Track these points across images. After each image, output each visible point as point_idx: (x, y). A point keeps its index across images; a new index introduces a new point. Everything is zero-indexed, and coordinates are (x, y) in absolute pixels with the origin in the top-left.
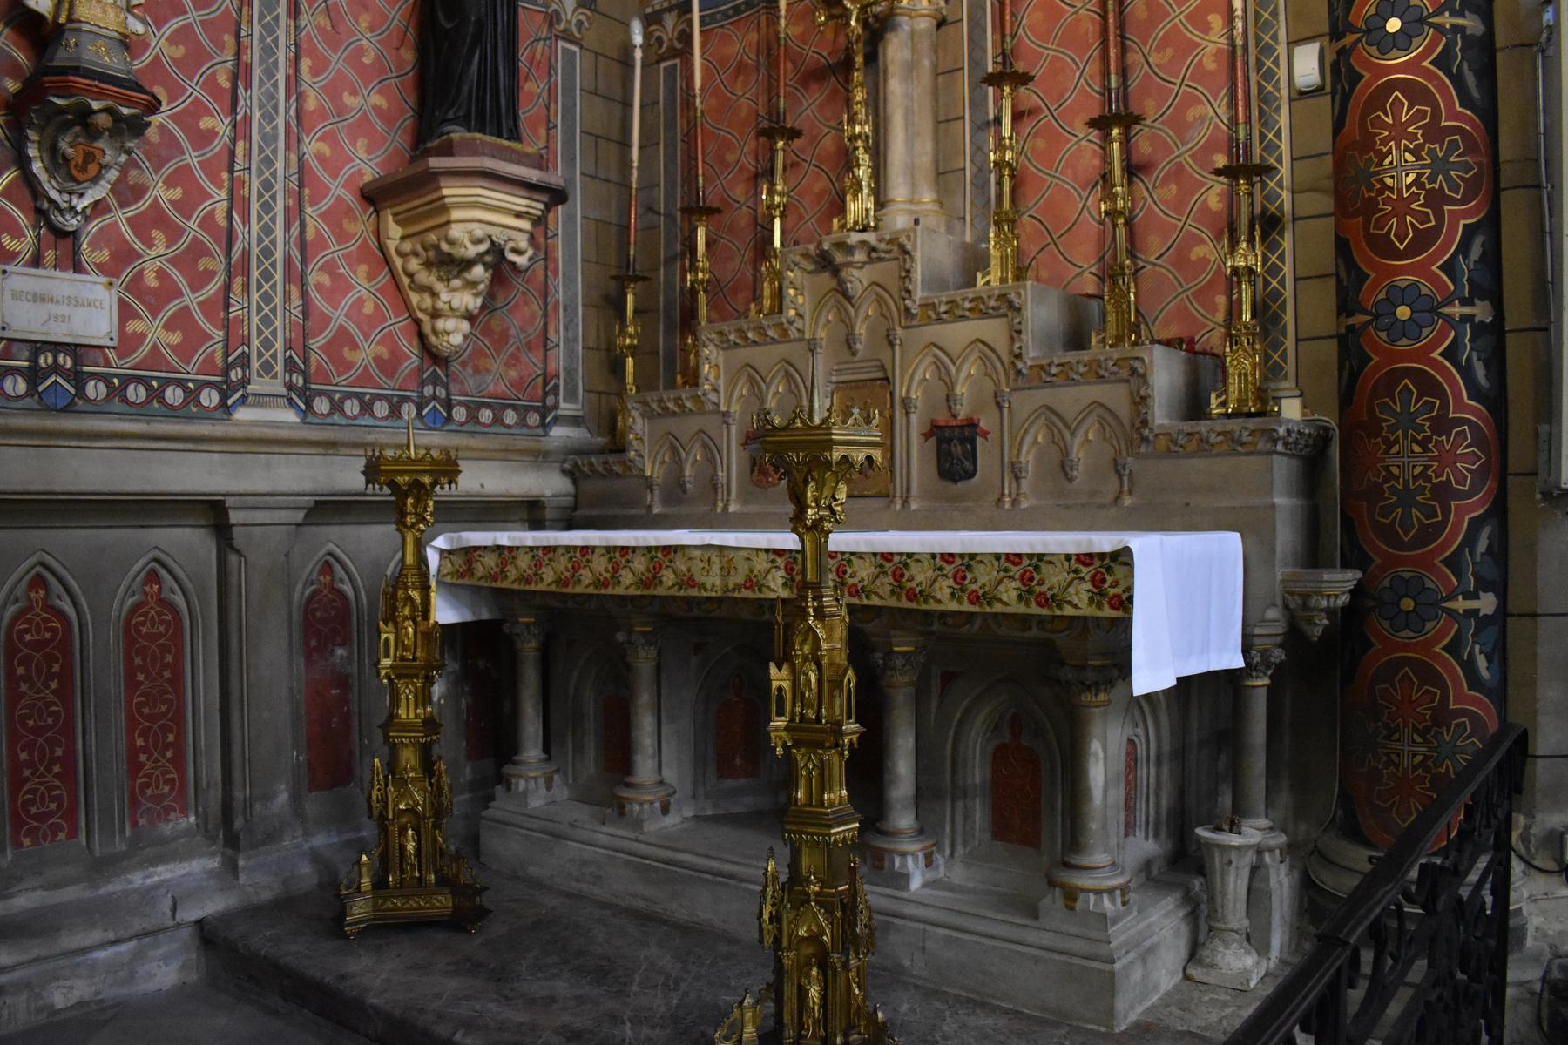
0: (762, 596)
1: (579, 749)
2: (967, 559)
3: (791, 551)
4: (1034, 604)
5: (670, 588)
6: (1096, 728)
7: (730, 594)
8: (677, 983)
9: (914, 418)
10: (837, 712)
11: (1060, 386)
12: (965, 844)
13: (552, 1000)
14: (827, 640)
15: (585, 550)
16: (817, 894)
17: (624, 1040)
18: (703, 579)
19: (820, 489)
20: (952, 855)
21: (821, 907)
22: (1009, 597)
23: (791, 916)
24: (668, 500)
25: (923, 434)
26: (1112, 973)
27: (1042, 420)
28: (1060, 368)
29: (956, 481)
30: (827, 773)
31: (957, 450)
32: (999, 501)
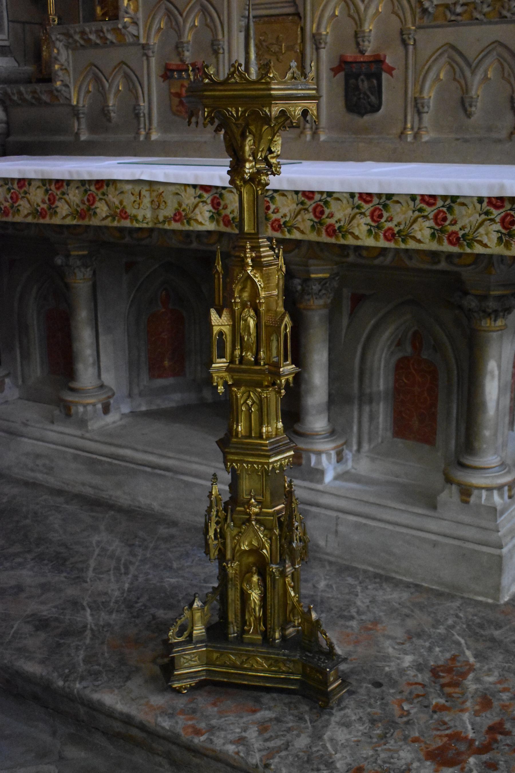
0: (191, 228)
1: (26, 356)
2: (384, 199)
3: (217, 187)
4: (446, 242)
5: (104, 219)
6: (493, 350)
7: (160, 226)
8: (126, 567)
9: (323, 53)
10: (274, 352)
11: (464, 25)
12: (370, 441)
13: (19, 589)
14: (266, 288)
15: (22, 182)
16: (257, 514)
17: (85, 627)
18: (134, 212)
19: (258, 140)
20: (359, 450)
21: (261, 526)
22: (423, 235)
23: (235, 532)
24: (93, 128)
25: (332, 69)
26: (500, 557)
27: (444, 59)
28: (465, 8)
29: (362, 115)
30: (265, 409)
31: (364, 85)
32: (402, 135)
